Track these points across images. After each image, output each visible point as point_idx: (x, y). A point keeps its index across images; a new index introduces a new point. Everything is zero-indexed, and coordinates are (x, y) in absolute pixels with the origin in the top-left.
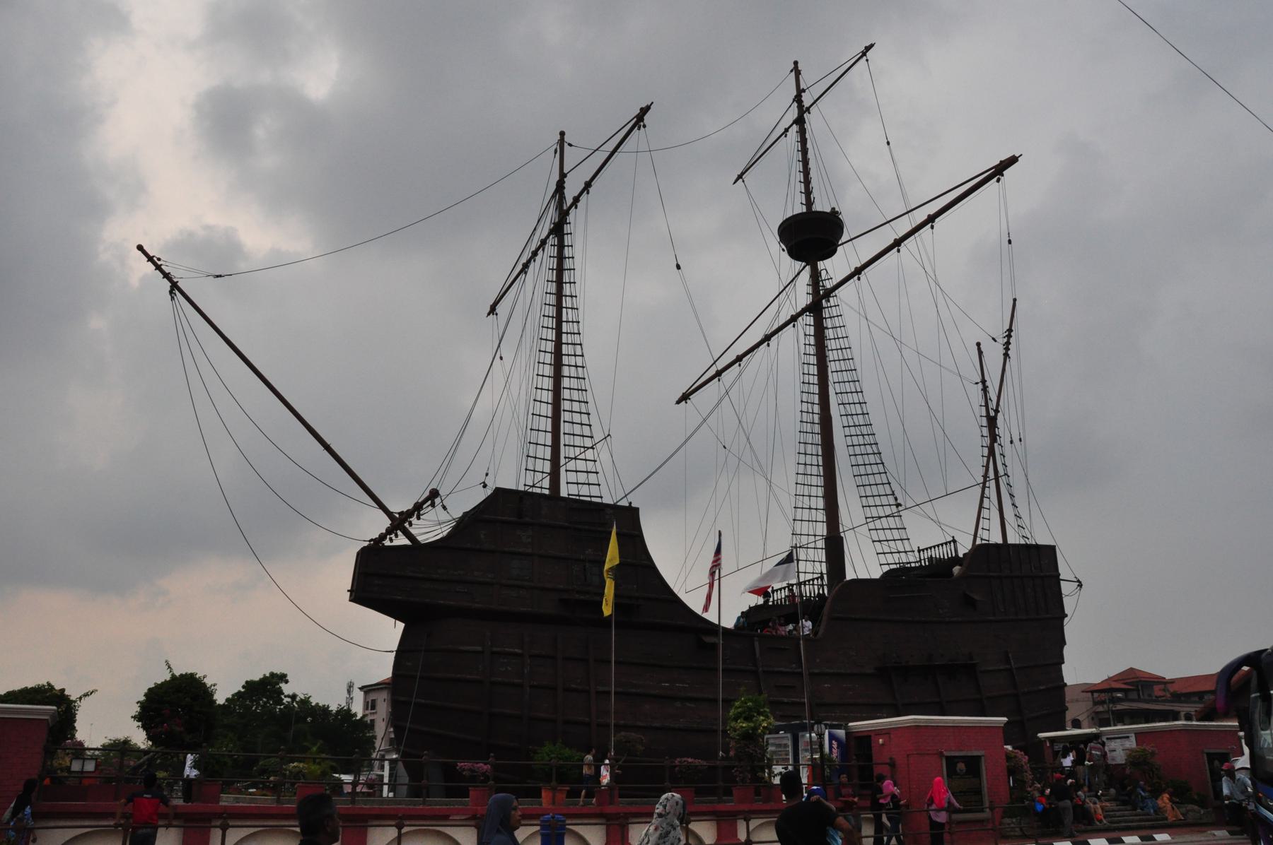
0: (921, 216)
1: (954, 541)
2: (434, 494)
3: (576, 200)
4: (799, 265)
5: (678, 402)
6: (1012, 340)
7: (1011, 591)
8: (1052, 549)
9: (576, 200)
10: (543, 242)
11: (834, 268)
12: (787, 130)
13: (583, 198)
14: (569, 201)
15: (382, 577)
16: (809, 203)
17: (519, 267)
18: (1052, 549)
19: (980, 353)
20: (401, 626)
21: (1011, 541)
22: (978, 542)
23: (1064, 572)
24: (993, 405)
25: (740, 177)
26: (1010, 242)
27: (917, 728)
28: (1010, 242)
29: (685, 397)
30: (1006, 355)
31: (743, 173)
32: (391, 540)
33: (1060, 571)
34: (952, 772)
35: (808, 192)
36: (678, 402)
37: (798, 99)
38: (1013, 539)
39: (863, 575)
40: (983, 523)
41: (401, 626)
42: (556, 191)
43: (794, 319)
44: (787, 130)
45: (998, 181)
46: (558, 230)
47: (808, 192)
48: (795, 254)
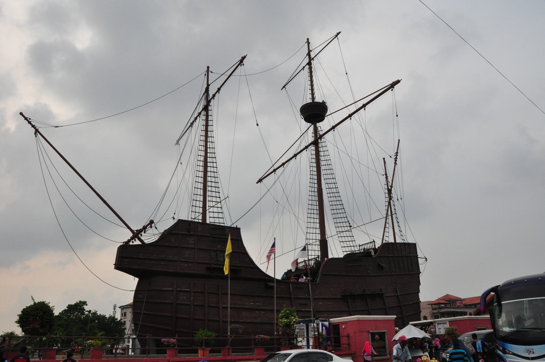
0: (360, 104)
1: (374, 242)
3: (214, 96)
4: (309, 124)
5: (257, 183)
8: (414, 245)
9: (214, 96)
10: (200, 114)
11: (323, 126)
12: (304, 67)
14: (211, 96)
16: (313, 98)
18: (414, 245)
20: (137, 279)
21: (397, 242)
22: (384, 242)
24: (390, 184)
25: (284, 87)
26: (397, 116)
28: (397, 116)
29: (260, 181)
30: (395, 163)
31: (285, 85)
34: (373, 339)
36: (257, 183)
38: (399, 240)
39: (336, 256)
41: (137, 279)
43: (306, 147)
44: (304, 67)
45: (392, 90)
46: (206, 108)
48: (307, 120)
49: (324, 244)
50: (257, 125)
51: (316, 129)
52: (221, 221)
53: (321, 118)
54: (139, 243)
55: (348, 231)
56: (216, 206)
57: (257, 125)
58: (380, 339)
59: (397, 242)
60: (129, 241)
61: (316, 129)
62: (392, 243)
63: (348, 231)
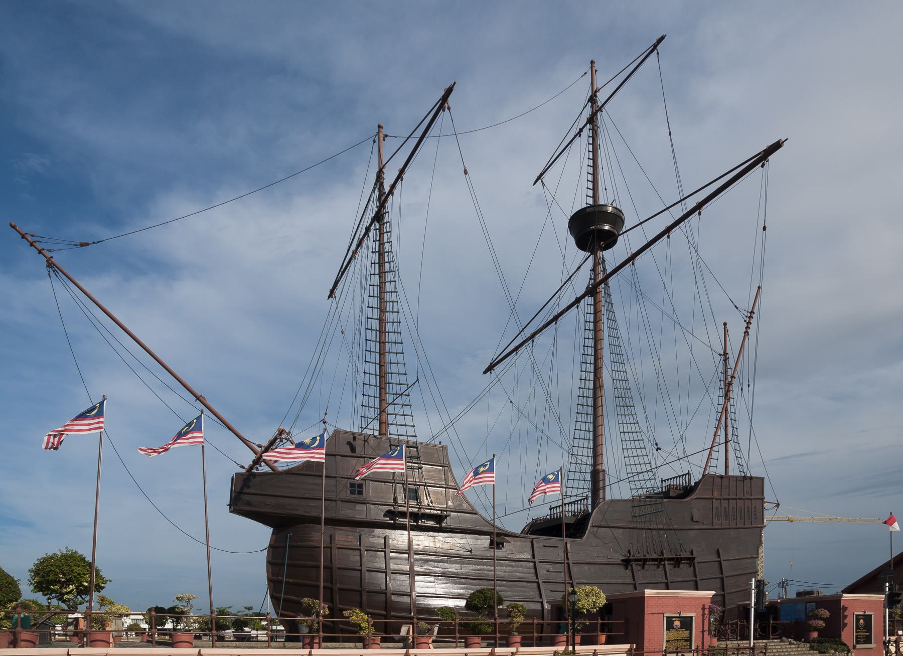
0: (691, 203)
1: (689, 474)
2: (281, 432)
3: (393, 187)
4: (583, 254)
5: (485, 372)
6: (752, 321)
7: (735, 501)
8: (762, 480)
9: (393, 187)
10: (368, 229)
11: (612, 256)
12: (581, 130)
13: (398, 185)
14: (387, 189)
15: (251, 495)
16: (595, 196)
17: (350, 254)
18: (762, 480)
19: (726, 330)
20: (270, 530)
21: (730, 473)
22: (707, 472)
23: (768, 495)
24: (730, 373)
25: (539, 178)
26: (764, 228)
27: (751, 589)
28: (764, 228)
29: (490, 368)
30: (746, 333)
31: (541, 175)
32: (257, 469)
33: (765, 495)
34: (670, 626)
35: (595, 189)
36: (485, 372)
37: (592, 99)
38: (734, 471)
39: (617, 497)
40: (713, 463)
41: (270, 530)
42: (377, 181)
43: (578, 301)
44: (581, 130)
45: (762, 166)
46: (379, 217)
47: (595, 189)
48: (582, 244)
49: (597, 477)
50: (466, 172)
51: (598, 263)
52: (410, 431)
53: (610, 240)
54: (268, 470)
55: (638, 473)
56: (395, 396)
57: (466, 172)
58: (681, 628)
59: (730, 473)
60: (251, 468)
61: (598, 263)
62: (721, 477)
63: (638, 473)
